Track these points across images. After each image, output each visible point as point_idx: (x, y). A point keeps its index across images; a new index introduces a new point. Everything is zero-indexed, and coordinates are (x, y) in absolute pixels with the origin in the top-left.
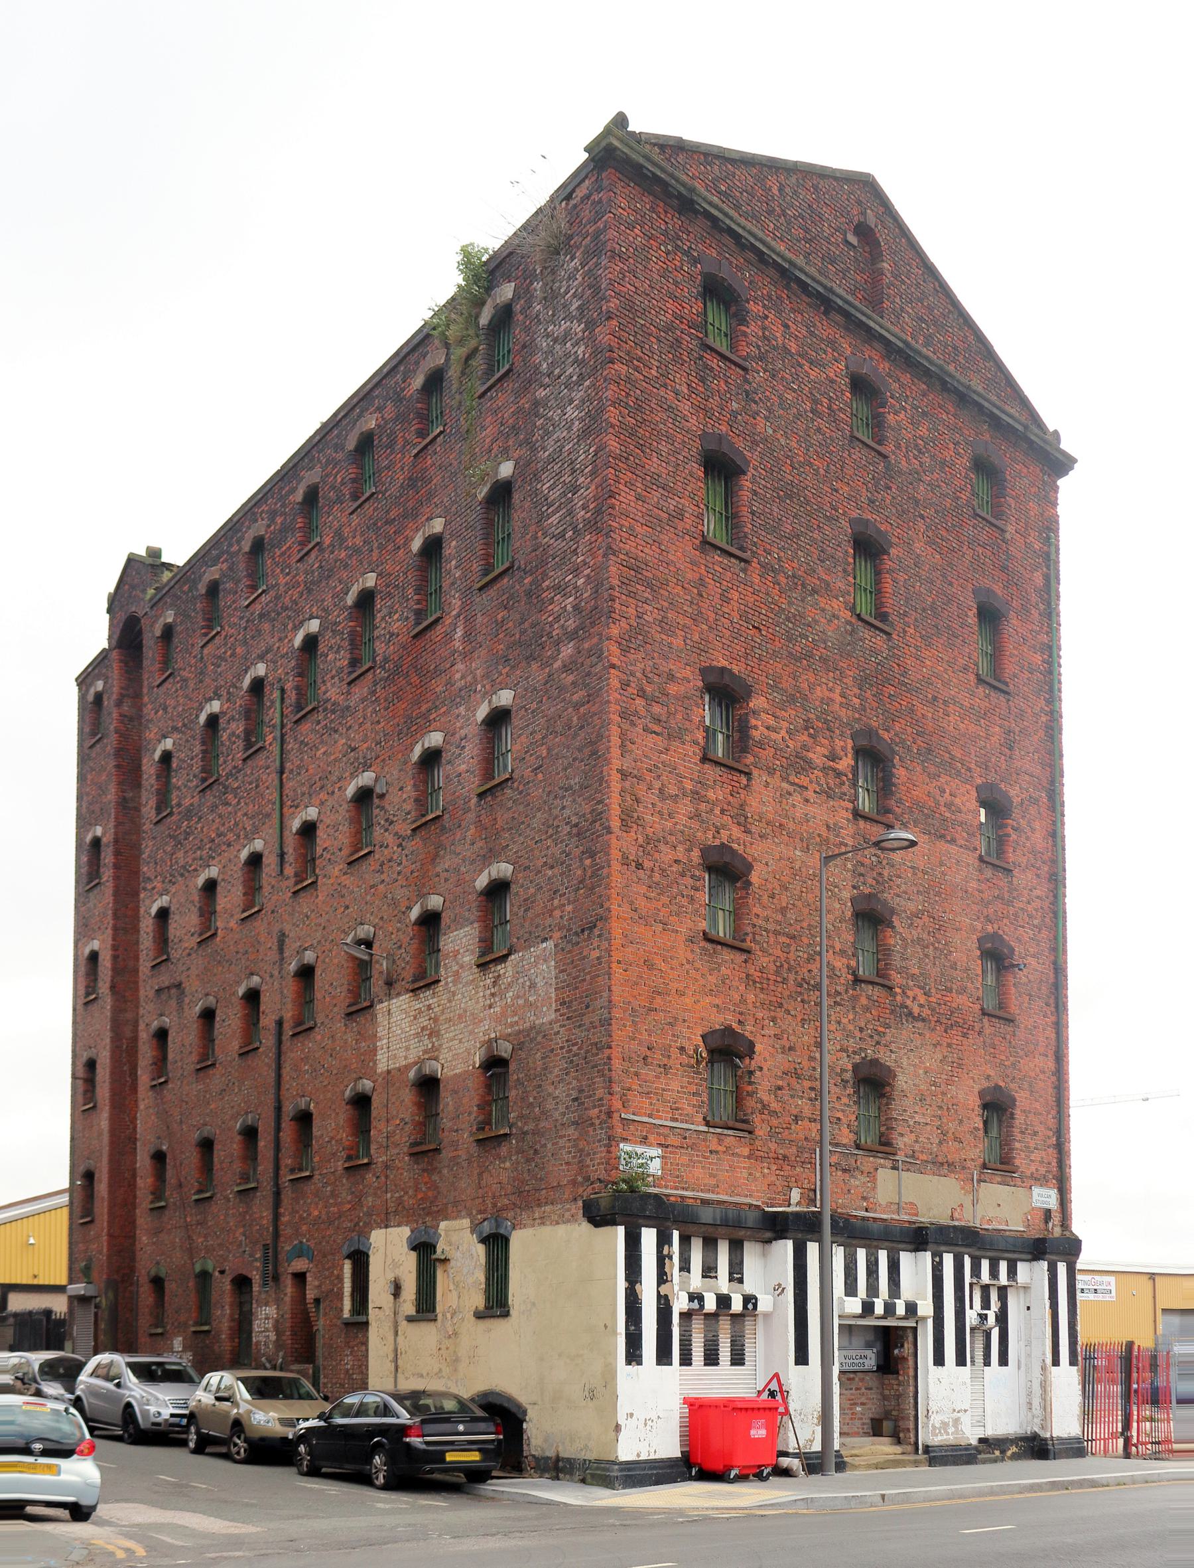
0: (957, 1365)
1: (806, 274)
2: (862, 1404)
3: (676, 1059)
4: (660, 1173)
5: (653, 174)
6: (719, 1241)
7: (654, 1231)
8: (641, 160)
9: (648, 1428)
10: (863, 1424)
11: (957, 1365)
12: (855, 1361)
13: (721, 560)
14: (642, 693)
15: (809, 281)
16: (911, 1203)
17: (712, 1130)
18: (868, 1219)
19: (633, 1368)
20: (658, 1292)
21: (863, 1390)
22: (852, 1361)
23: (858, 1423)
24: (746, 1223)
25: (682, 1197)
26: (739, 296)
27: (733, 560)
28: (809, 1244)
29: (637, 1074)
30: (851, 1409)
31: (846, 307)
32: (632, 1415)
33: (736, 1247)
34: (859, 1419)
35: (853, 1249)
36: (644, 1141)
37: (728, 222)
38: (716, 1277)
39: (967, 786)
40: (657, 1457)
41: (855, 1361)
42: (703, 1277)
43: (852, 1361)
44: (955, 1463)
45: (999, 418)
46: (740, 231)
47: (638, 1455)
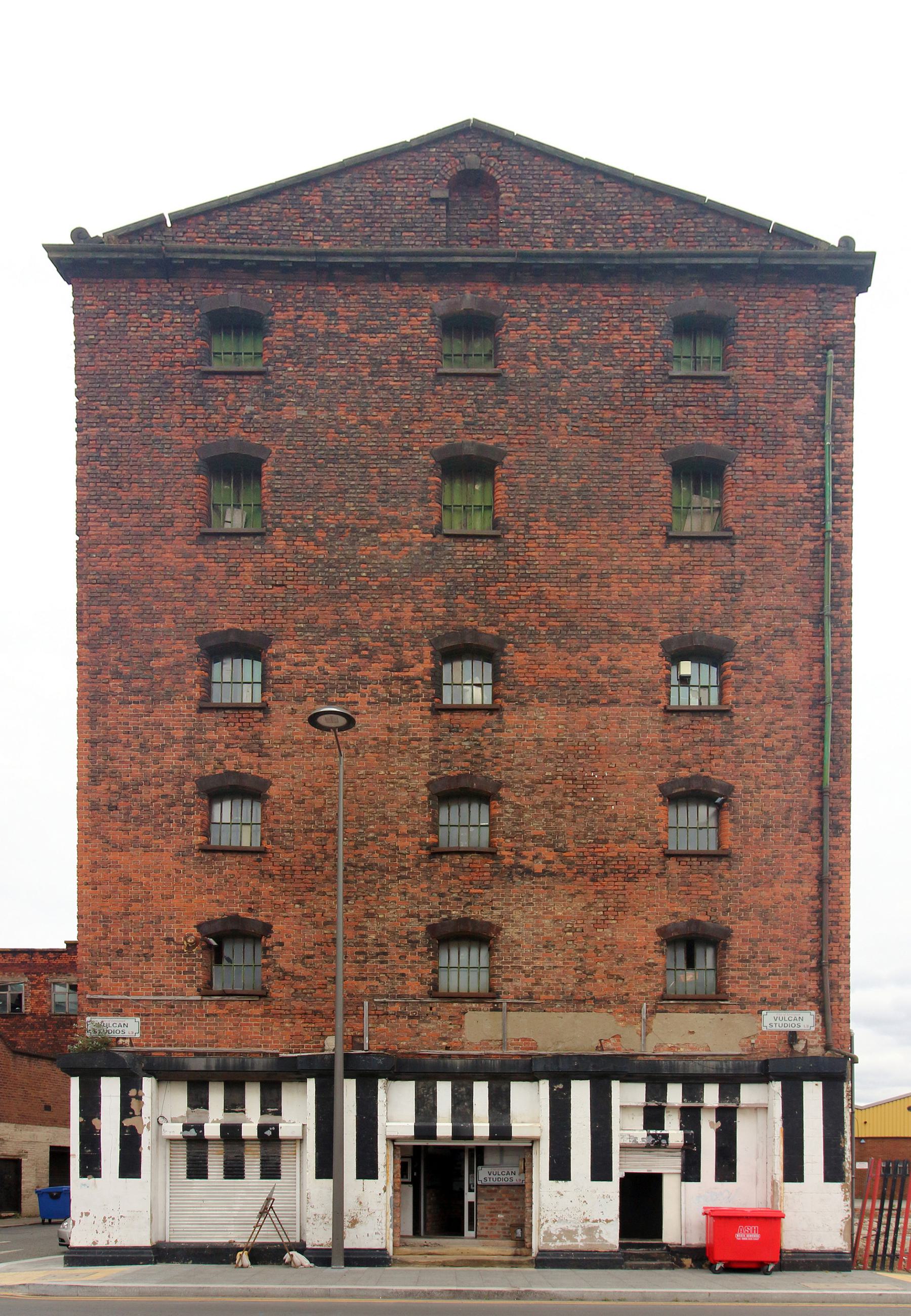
0: (717, 1180)
1: (342, 255)
2: (505, 1212)
3: (160, 947)
4: (138, 1036)
5: (147, 260)
6: (247, 1084)
7: (78, 1078)
8: (90, 255)
9: (108, 1223)
10: (505, 1229)
11: (717, 1180)
12: (501, 1176)
13: (227, 542)
14: (117, 675)
15: (350, 260)
16: (525, 1039)
17: (205, 998)
18: (450, 1056)
19: (90, 1181)
20: (122, 1124)
21: (507, 1200)
22: (497, 1176)
23: (499, 1228)
24: (252, 1067)
25: (169, 1052)
26: (259, 314)
27: (243, 538)
28: (104, 1080)
29: (109, 964)
30: (491, 1216)
31: (413, 260)
32: (87, 1214)
33: (130, 1084)
34: (500, 1224)
35: (430, 1083)
36: (118, 1013)
37: (218, 257)
38: (244, 1112)
39: (643, 646)
40: (118, 1245)
41: (501, 1176)
42: (225, 1111)
43: (497, 1176)
44: (553, 1267)
45: (709, 265)
46: (239, 257)
47: (94, 1243)
